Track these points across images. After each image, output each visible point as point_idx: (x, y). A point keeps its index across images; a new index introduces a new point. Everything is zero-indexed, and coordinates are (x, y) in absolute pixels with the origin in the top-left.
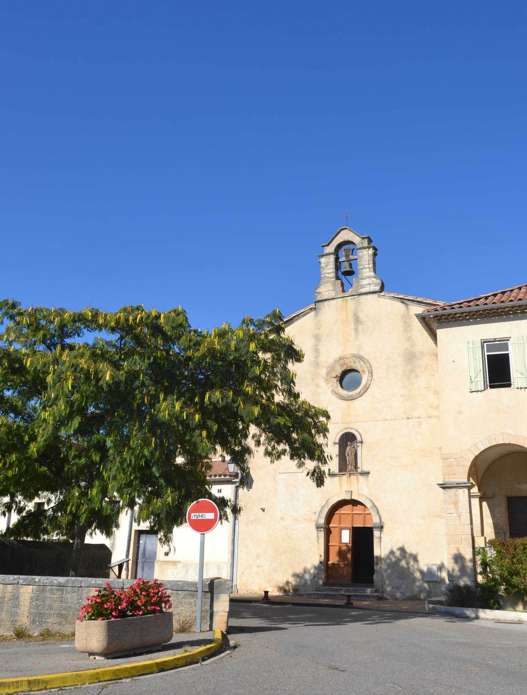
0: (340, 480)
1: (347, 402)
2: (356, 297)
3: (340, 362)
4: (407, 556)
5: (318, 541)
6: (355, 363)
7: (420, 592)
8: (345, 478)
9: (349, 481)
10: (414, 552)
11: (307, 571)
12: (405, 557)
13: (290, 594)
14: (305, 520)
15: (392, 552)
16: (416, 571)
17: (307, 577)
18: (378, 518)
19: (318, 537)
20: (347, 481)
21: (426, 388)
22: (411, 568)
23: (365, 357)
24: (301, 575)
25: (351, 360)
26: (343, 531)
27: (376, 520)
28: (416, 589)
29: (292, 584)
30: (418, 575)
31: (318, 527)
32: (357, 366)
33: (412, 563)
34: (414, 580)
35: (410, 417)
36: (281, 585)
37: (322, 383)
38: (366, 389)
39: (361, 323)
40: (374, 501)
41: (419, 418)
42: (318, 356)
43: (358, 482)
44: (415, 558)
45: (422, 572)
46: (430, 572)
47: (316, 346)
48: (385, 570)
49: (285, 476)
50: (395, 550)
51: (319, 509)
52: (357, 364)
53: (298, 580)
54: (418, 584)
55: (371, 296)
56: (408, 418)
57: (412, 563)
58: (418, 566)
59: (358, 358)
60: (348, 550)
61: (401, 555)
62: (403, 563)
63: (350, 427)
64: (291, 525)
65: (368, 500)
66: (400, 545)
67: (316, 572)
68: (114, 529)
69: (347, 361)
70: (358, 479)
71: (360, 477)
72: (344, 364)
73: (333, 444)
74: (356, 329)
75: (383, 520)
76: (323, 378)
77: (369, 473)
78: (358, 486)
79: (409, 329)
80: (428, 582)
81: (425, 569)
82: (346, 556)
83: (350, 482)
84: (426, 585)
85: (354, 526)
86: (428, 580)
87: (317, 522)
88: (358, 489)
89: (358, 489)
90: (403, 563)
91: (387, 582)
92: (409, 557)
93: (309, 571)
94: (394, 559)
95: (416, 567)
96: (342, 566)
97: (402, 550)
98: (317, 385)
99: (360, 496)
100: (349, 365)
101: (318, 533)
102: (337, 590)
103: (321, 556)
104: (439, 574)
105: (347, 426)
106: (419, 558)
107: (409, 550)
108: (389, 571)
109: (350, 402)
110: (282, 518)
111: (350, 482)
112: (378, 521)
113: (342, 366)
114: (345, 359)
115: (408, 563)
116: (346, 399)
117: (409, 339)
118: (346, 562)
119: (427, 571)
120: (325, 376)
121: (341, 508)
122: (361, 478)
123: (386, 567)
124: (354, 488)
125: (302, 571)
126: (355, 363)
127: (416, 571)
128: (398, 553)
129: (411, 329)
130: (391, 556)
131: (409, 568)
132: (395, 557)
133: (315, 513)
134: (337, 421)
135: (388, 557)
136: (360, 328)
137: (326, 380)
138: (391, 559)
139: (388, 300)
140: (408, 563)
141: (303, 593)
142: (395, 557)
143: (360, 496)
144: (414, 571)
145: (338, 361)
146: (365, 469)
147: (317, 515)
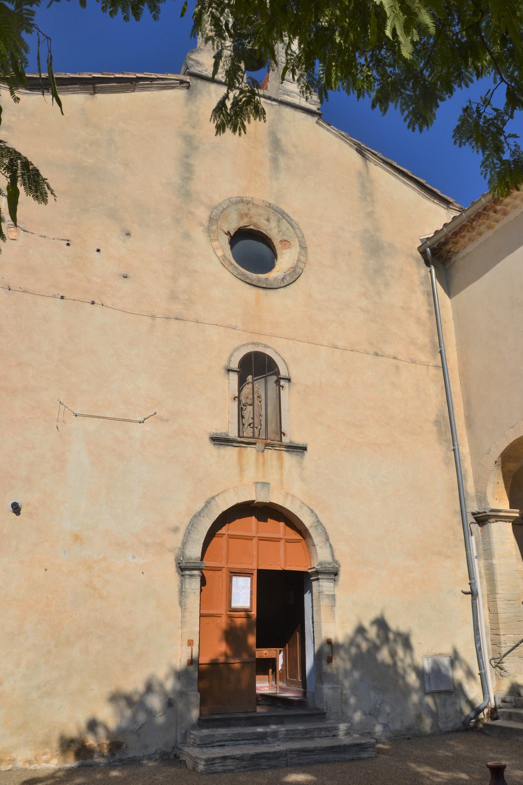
0: (240, 456)
1: (254, 290)
2: (274, 103)
3: (241, 206)
4: (391, 636)
5: (181, 604)
6: (268, 220)
7: (419, 717)
8: (251, 452)
9: (261, 460)
10: (403, 628)
11: (157, 688)
12: (386, 640)
13: (97, 759)
14: (147, 545)
15: (361, 630)
16: (409, 670)
17: (155, 702)
18: (328, 551)
19: (182, 592)
20: (257, 460)
21: (402, 308)
22: (399, 664)
23: (292, 216)
24: (136, 698)
25: (261, 211)
26: (235, 579)
27: (322, 555)
28: (412, 712)
29: (106, 728)
30: (412, 679)
31: (183, 568)
32: (271, 229)
33: (400, 652)
34: (407, 690)
35: (380, 353)
36: (72, 732)
37: (199, 235)
38: (294, 276)
39: (284, 153)
40: (316, 512)
41: (395, 358)
42: (189, 179)
43: (281, 467)
44: (407, 644)
45: (420, 673)
46: (437, 672)
47: (187, 157)
48: (347, 674)
49: (91, 425)
50: (366, 624)
51: (187, 520)
52: (273, 224)
53: (128, 713)
54: (415, 698)
55: (303, 115)
56: (376, 354)
57: (400, 652)
58: (412, 658)
59: (279, 213)
60: (249, 626)
61: (378, 636)
62: (384, 655)
63: (263, 342)
64: (104, 559)
65: (305, 508)
66: (374, 614)
67: (178, 686)
68: (434, 120)
69: (254, 211)
70: (280, 459)
71: (286, 456)
72: (246, 215)
73: (223, 371)
74: (274, 160)
75: (337, 558)
76: (201, 225)
77: (304, 449)
78: (282, 474)
79: (369, 198)
80: (432, 694)
81: (427, 665)
82: (245, 640)
83: (264, 463)
84: (429, 700)
85: (261, 568)
86: (433, 689)
87: (183, 554)
88: (281, 482)
89: (281, 482)
90: (384, 655)
91: (352, 701)
92: (395, 641)
93: (161, 686)
94: (364, 646)
95: (408, 660)
96: (237, 666)
97: (381, 623)
98: (187, 236)
99: (289, 498)
100: (255, 220)
101: (182, 583)
102: (262, 738)
103: (190, 643)
104: (450, 673)
105: (256, 339)
106: (414, 641)
107: (393, 624)
108: (356, 675)
109: (261, 291)
110: (77, 538)
111: (264, 463)
112: (329, 559)
113: (242, 216)
114: (250, 206)
115: (393, 654)
116: (255, 283)
117: (370, 214)
118: (245, 657)
119: (433, 669)
120: (206, 223)
121: (230, 522)
122: (289, 459)
123: (348, 665)
124: (273, 477)
125: (141, 687)
126: (268, 220)
127: (409, 670)
128: (372, 632)
129: (373, 201)
130: (360, 640)
131: (395, 664)
132: (367, 640)
133: (176, 530)
134: (234, 324)
135: (352, 642)
136: (282, 161)
137: (208, 231)
138: (358, 646)
139: (333, 137)
140: (393, 654)
141: (140, 754)
142: (367, 640)
143: (289, 498)
144: (405, 671)
145: (237, 203)
146: (298, 440)
147: (180, 536)
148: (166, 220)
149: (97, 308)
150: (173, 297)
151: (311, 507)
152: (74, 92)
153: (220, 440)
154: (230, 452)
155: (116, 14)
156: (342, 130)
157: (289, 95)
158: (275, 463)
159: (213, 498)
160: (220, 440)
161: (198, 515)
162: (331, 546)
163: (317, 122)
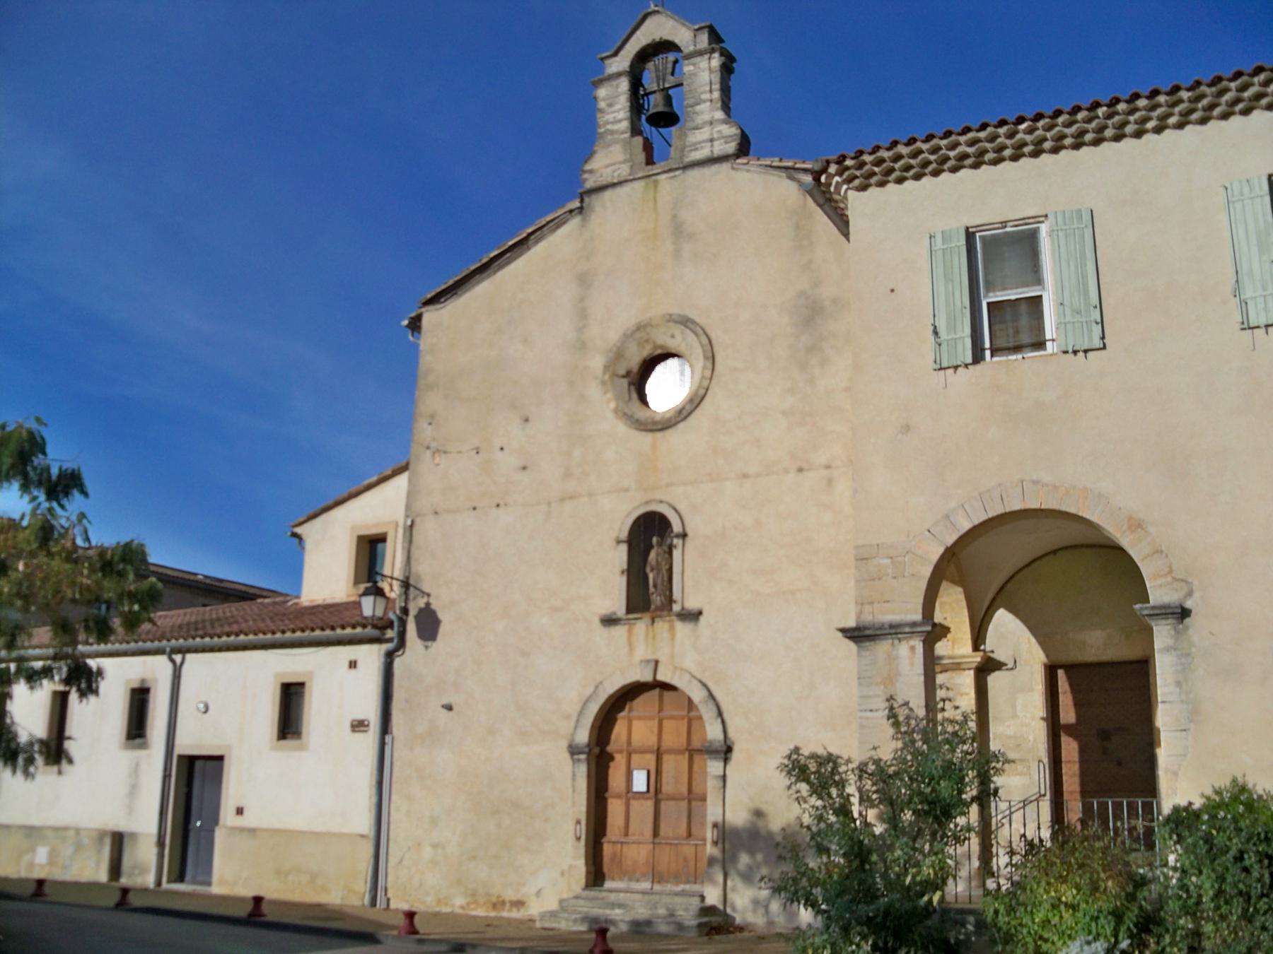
0: (630, 632)
2: (677, 173)
3: (638, 335)
6: (673, 336)
9: (651, 635)
18: (720, 727)
19: (574, 775)
40: (710, 685)
41: (828, 467)
42: (584, 326)
43: (673, 638)
70: (672, 629)
71: (679, 625)
83: (654, 638)
87: (573, 740)
88: (672, 656)
89: (672, 656)
105: (650, 496)
114: (649, 329)
122: (682, 628)
126: (673, 336)
145: (634, 332)
146: (692, 604)
148: (85, 572)
149: (501, 509)
150: (568, 474)
151: (704, 680)
152: (479, 282)
153: (609, 621)
154: (619, 631)
155: (132, 541)
156: (766, 156)
157: (696, 149)
158: (666, 635)
159: (601, 683)
160: (609, 621)
161: (587, 701)
162: (723, 722)
163: (733, 168)
